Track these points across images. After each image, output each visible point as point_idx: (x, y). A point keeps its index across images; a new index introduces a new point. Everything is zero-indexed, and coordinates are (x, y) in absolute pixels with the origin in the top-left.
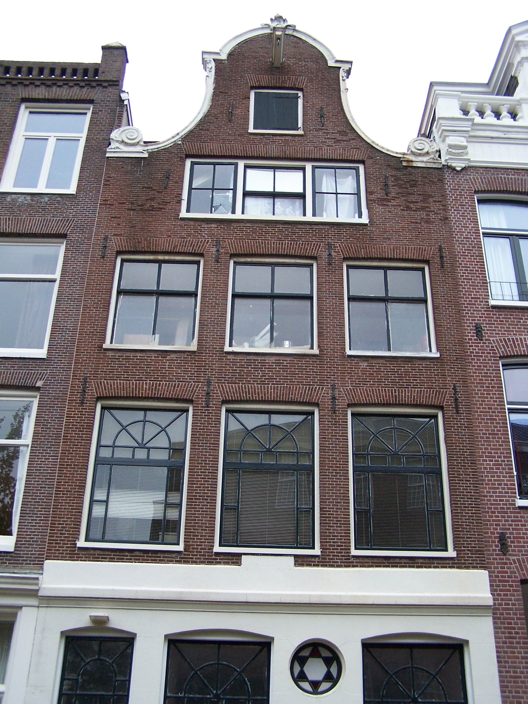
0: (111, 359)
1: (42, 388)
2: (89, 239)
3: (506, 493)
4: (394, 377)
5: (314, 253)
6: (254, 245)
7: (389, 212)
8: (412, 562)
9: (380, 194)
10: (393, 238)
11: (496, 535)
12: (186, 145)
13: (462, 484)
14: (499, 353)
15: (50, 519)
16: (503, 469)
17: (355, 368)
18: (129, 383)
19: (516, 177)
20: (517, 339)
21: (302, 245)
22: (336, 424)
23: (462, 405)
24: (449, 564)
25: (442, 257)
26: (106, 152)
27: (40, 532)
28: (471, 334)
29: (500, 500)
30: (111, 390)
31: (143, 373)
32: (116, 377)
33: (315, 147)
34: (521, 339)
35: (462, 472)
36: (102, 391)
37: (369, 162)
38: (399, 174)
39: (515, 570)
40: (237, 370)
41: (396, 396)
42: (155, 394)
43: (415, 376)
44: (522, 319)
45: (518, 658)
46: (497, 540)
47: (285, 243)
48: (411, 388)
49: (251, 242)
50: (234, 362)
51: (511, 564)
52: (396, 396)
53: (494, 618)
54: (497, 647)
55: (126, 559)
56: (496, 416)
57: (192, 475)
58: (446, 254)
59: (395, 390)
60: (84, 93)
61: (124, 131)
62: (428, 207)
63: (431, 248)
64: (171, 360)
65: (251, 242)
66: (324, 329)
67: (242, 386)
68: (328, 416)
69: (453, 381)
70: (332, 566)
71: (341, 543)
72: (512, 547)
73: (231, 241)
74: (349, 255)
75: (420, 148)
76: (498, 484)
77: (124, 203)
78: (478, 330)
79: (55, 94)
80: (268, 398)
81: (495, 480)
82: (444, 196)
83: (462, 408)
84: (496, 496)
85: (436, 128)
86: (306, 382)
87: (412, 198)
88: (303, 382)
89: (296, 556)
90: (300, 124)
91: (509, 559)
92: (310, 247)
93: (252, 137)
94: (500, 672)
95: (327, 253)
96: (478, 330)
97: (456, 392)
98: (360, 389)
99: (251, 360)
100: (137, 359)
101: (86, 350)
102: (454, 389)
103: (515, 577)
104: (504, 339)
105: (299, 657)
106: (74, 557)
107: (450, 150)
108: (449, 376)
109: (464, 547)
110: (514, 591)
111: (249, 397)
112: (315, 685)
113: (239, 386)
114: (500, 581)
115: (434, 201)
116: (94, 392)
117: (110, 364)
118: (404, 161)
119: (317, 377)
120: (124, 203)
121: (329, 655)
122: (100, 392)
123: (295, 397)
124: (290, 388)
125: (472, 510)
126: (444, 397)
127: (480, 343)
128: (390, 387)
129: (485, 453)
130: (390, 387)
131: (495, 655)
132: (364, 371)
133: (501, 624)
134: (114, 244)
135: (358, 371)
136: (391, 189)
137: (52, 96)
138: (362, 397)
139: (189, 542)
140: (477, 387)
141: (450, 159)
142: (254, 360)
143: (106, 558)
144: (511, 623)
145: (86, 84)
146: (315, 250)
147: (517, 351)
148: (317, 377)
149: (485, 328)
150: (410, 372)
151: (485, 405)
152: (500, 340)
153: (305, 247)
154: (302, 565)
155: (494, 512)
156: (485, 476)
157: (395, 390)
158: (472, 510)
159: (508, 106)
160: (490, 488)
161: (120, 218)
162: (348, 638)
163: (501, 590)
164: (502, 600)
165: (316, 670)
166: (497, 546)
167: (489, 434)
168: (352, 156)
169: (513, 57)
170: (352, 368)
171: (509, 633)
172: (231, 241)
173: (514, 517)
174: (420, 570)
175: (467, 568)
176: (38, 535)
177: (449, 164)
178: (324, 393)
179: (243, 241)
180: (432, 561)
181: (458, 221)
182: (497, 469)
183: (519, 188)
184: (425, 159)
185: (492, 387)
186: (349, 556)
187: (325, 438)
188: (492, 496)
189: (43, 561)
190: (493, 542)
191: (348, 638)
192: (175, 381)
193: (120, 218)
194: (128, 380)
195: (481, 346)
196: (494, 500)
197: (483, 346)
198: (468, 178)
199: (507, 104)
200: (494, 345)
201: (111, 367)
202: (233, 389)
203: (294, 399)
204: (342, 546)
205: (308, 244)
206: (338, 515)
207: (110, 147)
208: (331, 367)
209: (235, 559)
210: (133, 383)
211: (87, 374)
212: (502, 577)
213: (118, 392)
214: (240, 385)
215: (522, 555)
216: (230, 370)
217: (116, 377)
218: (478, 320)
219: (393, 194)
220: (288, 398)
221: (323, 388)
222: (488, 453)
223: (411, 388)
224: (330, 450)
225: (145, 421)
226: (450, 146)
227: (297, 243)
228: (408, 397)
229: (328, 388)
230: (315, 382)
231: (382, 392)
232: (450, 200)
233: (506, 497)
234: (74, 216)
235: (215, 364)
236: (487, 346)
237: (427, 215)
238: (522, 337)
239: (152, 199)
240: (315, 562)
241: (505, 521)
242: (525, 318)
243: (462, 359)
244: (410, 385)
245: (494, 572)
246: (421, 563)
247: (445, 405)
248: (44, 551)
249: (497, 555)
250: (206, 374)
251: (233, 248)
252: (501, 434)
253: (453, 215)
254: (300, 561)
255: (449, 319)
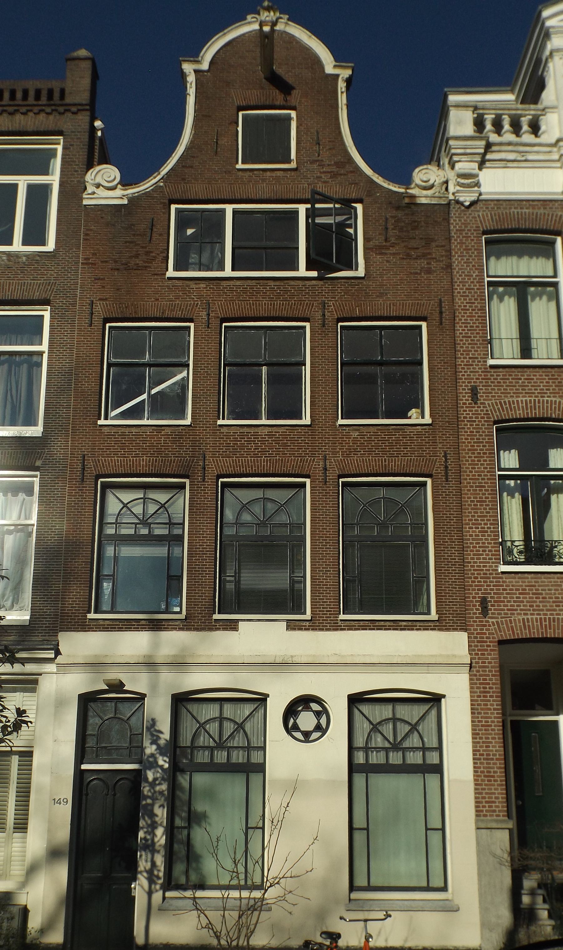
0: (107, 435)
1: (42, 467)
2: (74, 305)
3: (490, 559)
4: (385, 446)
5: (307, 314)
6: (245, 308)
7: (387, 261)
8: (396, 626)
9: (379, 240)
10: (389, 293)
11: (477, 599)
12: (169, 188)
13: (447, 551)
14: (494, 417)
15: (60, 594)
16: (489, 536)
17: (346, 438)
18: (127, 460)
19: (531, 210)
20: (513, 401)
21: (294, 305)
22: (327, 496)
23: (452, 473)
24: (431, 626)
25: (441, 313)
26: (82, 199)
27: (52, 606)
28: (465, 398)
29: (484, 566)
30: (110, 467)
31: (139, 449)
32: (114, 454)
33: (308, 184)
34: (517, 401)
35: (448, 539)
36: (101, 468)
37: (367, 200)
38: (400, 214)
39: (494, 631)
40: (401, 448)
41: (385, 465)
42: (152, 470)
43: (405, 445)
44: (520, 379)
45: (490, 709)
46: (477, 604)
47: (277, 303)
48: (401, 456)
49: (241, 303)
50: (228, 435)
51: (490, 626)
52: (385, 465)
53: (470, 675)
54: (471, 701)
55: (134, 628)
56: (485, 483)
57: (191, 548)
58: (446, 306)
59: (385, 460)
60: (50, 122)
61: (100, 171)
62: (430, 254)
63: (430, 303)
64: (165, 435)
65: (241, 303)
66: (316, 398)
67: (236, 460)
68: (319, 487)
69: (444, 448)
70: (322, 630)
71: (330, 608)
72: (492, 610)
73: (221, 303)
74: (343, 315)
75: (425, 179)
76: (483, 551)
77: (106, 262)
78: (474, 392)
79: (20, 124)
80: (261, 471)
81: (479, 547)
82: (449, 239)
83: (452, 476)
84: (480, 563)
85: (445, 151)
86: (298, 454)
87: (413, 243)
88: (295, 454)
89: (288, 621)
90: (293, 155)
91: (488, 622)
92: (303, 307)
93: (240, 173)
94: (472, 721)
95: (321, 313)
96: (474, 392)
97: (446, 459)
98: (350, 460)
99: (244, 433)
100: (132, 435)
101: (81, 427)
102: (445, 456)
103: (493, 638)
104: (500, 403)
105: (291, 711)
106: (86, 628)
107: (459, 180)
108: (440, 443)
109: (446, 611)
110: (491, 650)
111: (243, 470)
112: (307, 735)
113: (233, 460)
114: (478, 642)
115: (437, 246)
116: (92, 470)
117: (106, 441)
118: (407, 197)
119: (309, 449)
120: (106, 262)
121: (320, 708)
122: (98, 470)
123: (287, 469)
124: (282, 460)
125: (456, 576)
126: (434, 465)
127: (474, 407)
128: (381, 457)
129: (472, 520)
130: (381, 457)
131: (469, 707)
132: (355, 441)
133: (477, 680)
134: (100, 310)
135: (349, 441)
136: (391, 233)
137: (16, 127)
138: (352, 467)
139: (191, 610)
140: (468, 453)
141: (458, 191)
142: (247, 433)
143: (115, 628)
144: (485, 680)
145: (53, 110)
146: (308, 311)
147: (505, 415)
148: (309, 449)
149: (481, 391)
150: (401, 440)
151: (475, 472)
152: (496, 403)
153: (297, 307)
154: (294, 629)
155: (477, 578)
156: (471, 543)
157: (385, 460)
158: (456, 576)
159: (530, 117)
160: (474, 555)
161: (103, 279)
162: (335, 693)
163: (479, 650)
164: (479, 658)
165: (307, 720)
166: (477, 610)
167: (477, 501)
168: (349, 194)
169: (543, 47)
170: (343, 438)
171: (484, 688)
172: (221, 303)
173: (496, 582)
174: (403, 632)
175: (448, 630)
176: (50, 609)
177: (457, 198)
178: (315, 465)
179: (233, 303)
180: (414, 623)
181: (461, 269)
182: (482, 536)
183: (533, 224)
184: (430, 193)
185: (484, 453)
186: (338, 620)
187: (316, 509)
188: (476, 563)
189: (57, 633)
190: (475, 606)
191: (335, 693)
192: (171, 457)
193: (103, 279)
194: (125, 457)
195: (476, 411)
196: (477, 566)
197: (477, 411)
198: (476, 216)
199: (529, 115)
200: (488, 409)
201: (107, 443)
202: (227, 463)
203: (286, 471)
204: (331, 611)
205: (301, 304)
206: (328, 582)
207: (86, 193)
208: (322, 438)
209: (232, 626)
210: (130, 460)
211: (84, 452)
212: (480, 638)
213: (116, 470)
214: (234, 459)
215: (501, 618)
216: (322, 438)
217: (114, 454)
218: (474, 382)
219: (393, 240)
220: (281, 471)
221: (314, 460)
222: (475, 520)
223: (401, 456)
224: (321, 520)
225: (144, 499)
226: (460, 176)
227: (289, 303)
228: (398, 466)
229: (320, 459)
230: (307, 454)
231: (373, 462)
232: (454, 245)
233: (489, 563)
234: (56, 279)
235: (209, 438)
236: (481, 411)
237: (428, 264)
238: (519, 399)
239: (137, 256)
240: (306, 626)
241: (487, 586)
242: (562, 369)
243: (455, 423)
244: (401, 454)
245: (473, 634)
246: (405, 626)
247: (435, 473)
248: (58, 624)
249: (477, 618)
250: (200, 449)
251: (223, 311)
252: (489, 501)
253: (456, 261)
254: (292, 626)
255: (444, 382)
